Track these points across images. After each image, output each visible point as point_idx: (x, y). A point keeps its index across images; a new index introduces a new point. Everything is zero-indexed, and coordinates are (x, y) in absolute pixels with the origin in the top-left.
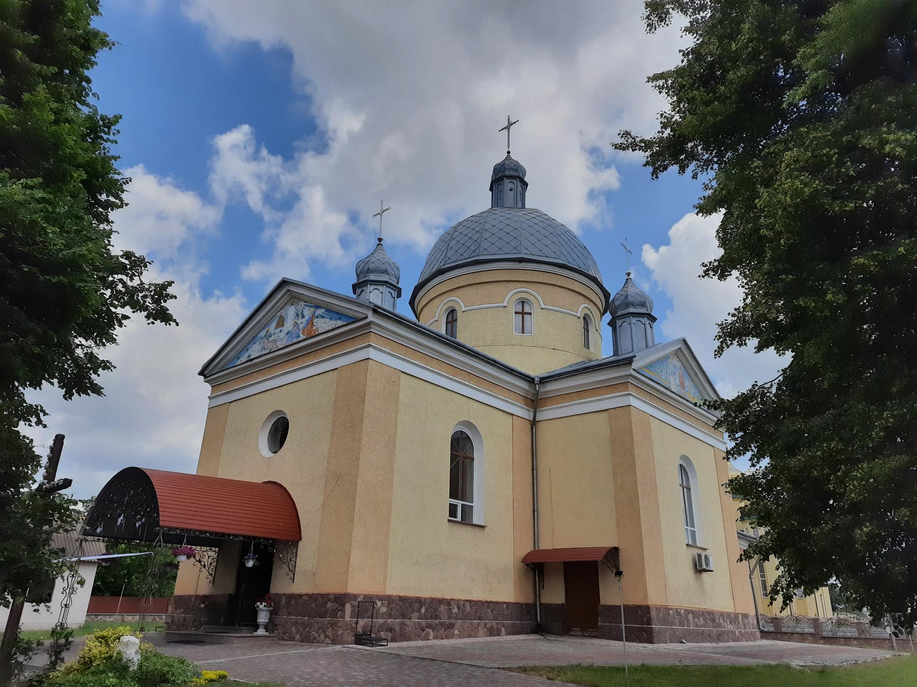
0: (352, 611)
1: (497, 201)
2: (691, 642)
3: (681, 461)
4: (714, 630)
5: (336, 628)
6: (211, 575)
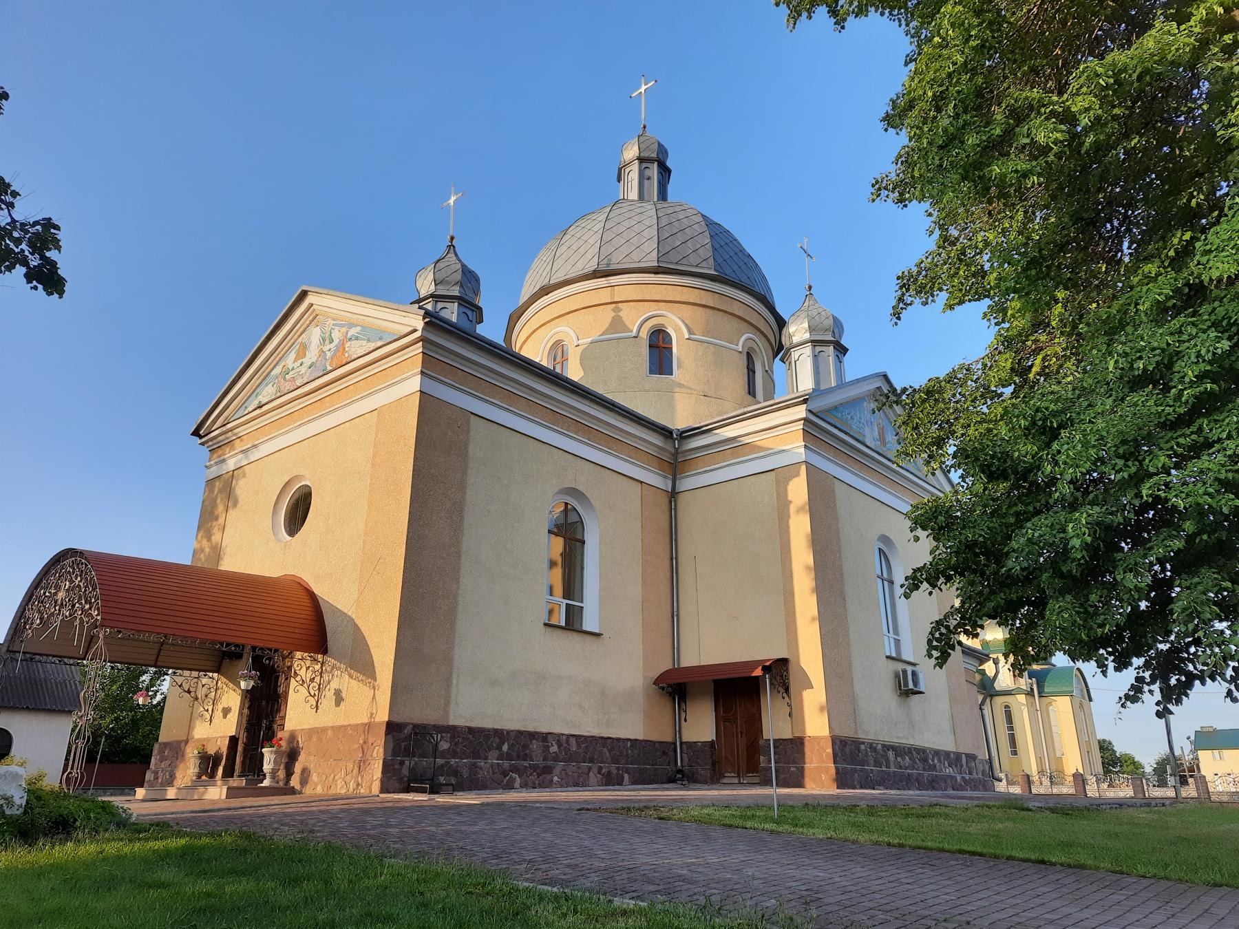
0: (394, 746)
2: (891, 789)
3: (880, 544)
4: (926, 774)
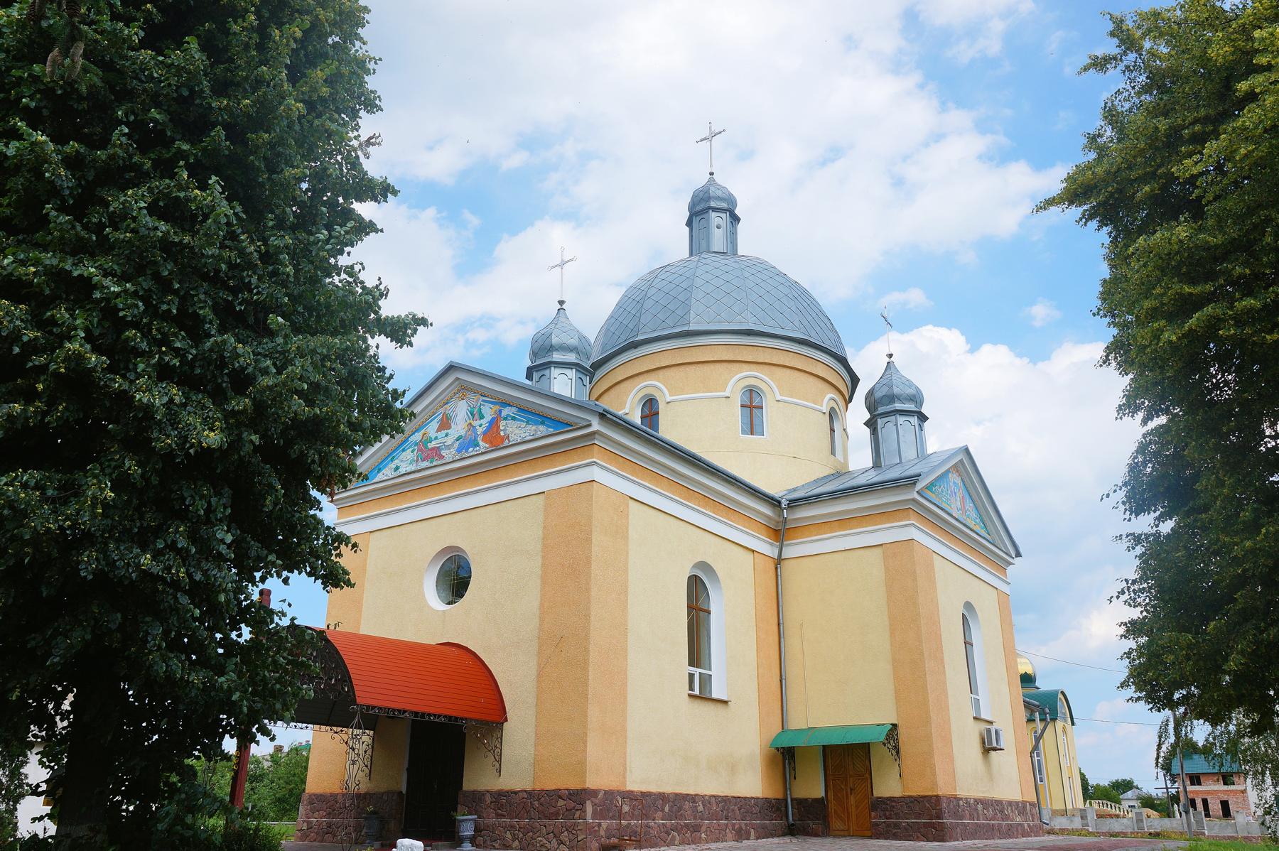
1: (698, 244)
5: (574, 832)
6: (367, 766)
